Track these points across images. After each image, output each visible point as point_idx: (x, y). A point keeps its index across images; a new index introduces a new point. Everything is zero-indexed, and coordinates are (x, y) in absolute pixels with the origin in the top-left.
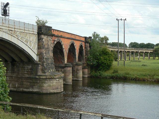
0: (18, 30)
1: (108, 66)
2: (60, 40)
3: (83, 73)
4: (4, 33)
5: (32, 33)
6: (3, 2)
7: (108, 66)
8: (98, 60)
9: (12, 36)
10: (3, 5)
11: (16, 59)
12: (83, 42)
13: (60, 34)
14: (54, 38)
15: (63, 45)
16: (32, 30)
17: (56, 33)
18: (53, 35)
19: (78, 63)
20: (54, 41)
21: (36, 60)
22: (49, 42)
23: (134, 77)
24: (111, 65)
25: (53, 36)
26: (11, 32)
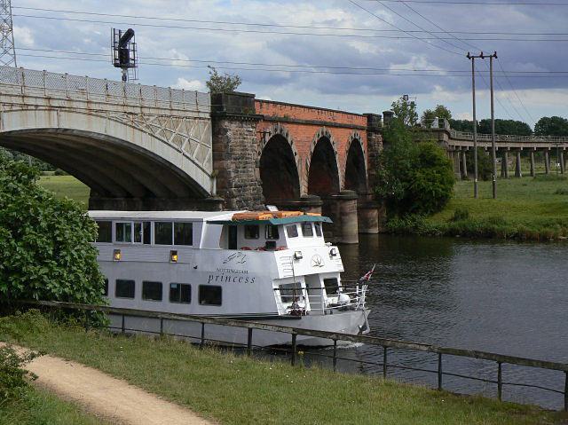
0: (152, 111)
1: (438, 199)
2: (281, 131)
3: (364, 223)
4: (112, 122)
5: (196, 115)
6: (117, 28)
7: (438, 199)
8: (409, 181)
9: (134, 127)
10: (117, 37)
11: (156, 190)
12: (362, 129)
13: (281, 113)
14: (261, 125)
15: (292, 143)
16: (194, 108)
17: (267, 112)
18: (256, 119)
19: (347, 193)
20: (265, 133)
21: (209, 191)
22: (247, 140)
23: (516, 230)
24: (447, 196)
25: (260, 119)
26: (132, 117)
